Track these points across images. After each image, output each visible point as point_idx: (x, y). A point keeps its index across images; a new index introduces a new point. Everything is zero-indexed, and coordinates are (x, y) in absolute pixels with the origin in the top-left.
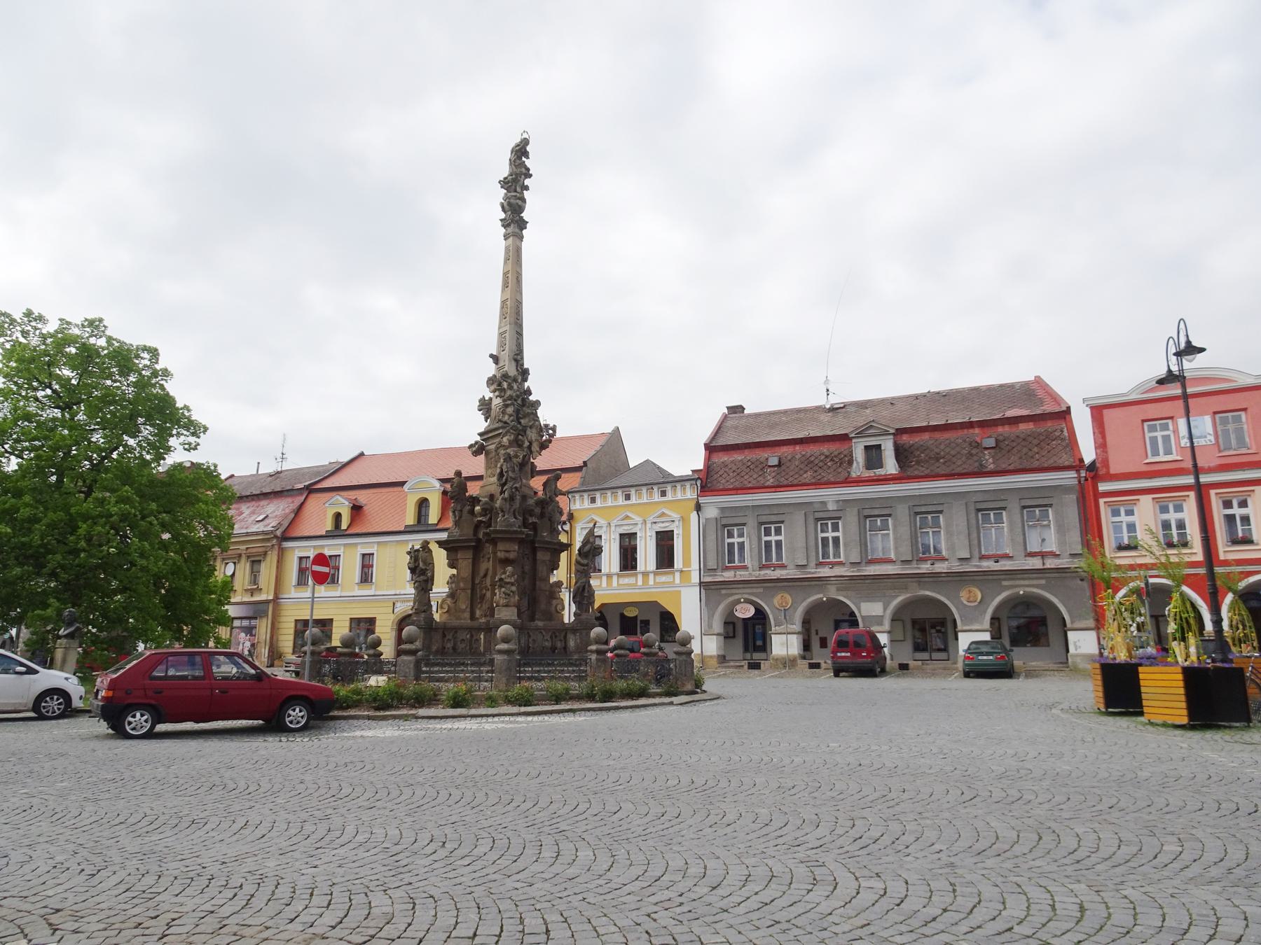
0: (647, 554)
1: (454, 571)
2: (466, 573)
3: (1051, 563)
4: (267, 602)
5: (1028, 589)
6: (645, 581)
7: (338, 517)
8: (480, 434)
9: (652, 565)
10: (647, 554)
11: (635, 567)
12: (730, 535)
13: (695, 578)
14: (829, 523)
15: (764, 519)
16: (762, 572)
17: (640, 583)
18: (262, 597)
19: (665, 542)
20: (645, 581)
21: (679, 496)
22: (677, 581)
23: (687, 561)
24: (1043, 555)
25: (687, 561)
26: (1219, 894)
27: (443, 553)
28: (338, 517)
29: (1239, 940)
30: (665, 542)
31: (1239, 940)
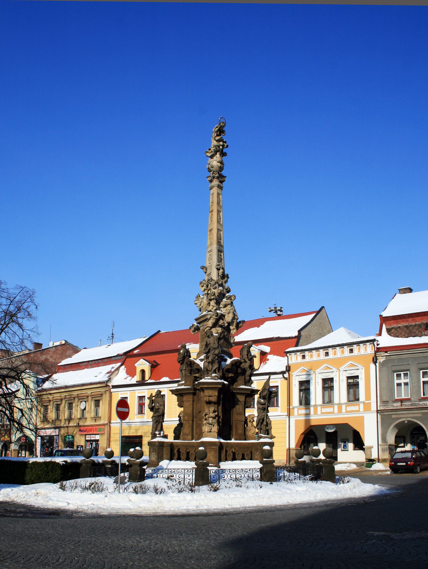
0: (340, 391)
1: (182, 409)
2: (189, 411)
3: (407, 405)
4: (104, 425)
5: (409, 419)
6: (340, 411)
7: (143, 372)
8: (196, 320)
9: (344, 399)
10: (340, 391)
11: (358, 400)
12: (399, 376)
13: (374, 408)
14: (402, 373)
15: (394, 368)
16: (421, 403)
17: (336, 411)
18: (102, 422)
19: (353, 384)
20: (340, 411)
21: (362, 351)
22: (362, 409)
23: (368, 396)
24: (402, 401)
25: (368, 396)
26: (51, 499)
27: (175, 398)
28: (143, 372)
29: (311, 568)
30: (353, 384)
31: (311, 568)
